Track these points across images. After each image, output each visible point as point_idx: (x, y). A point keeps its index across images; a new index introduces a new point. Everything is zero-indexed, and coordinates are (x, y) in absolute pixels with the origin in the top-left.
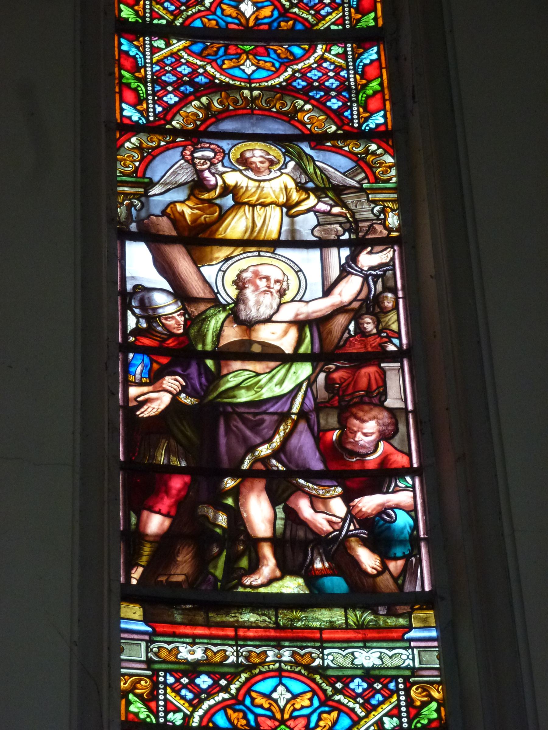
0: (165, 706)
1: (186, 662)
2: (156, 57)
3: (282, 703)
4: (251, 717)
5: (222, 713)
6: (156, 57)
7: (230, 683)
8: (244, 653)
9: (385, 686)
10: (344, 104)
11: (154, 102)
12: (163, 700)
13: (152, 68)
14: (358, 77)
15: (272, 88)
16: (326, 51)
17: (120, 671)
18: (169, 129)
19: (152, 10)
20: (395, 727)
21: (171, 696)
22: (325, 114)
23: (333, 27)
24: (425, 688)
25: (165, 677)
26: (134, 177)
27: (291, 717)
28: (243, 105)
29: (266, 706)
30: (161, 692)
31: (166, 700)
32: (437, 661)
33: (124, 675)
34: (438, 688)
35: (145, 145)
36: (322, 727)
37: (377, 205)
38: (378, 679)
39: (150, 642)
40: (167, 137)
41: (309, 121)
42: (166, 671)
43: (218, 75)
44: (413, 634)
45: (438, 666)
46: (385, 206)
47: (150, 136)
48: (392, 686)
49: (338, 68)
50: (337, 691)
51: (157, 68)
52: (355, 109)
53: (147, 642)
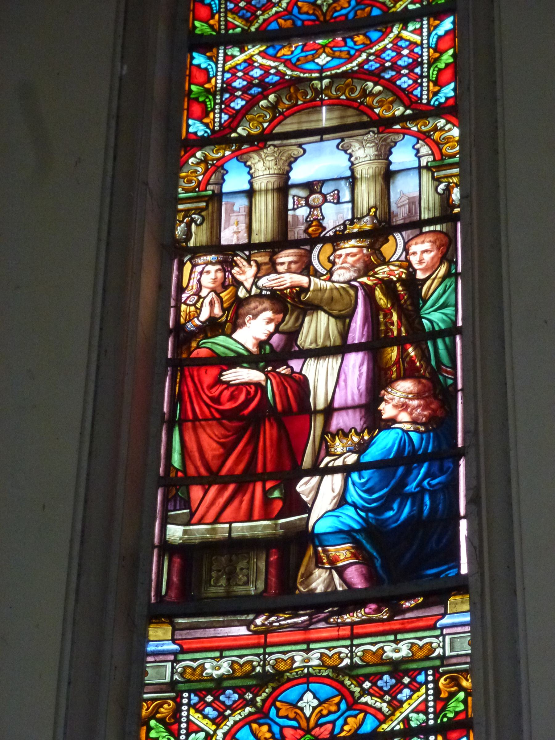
0: (187, 729)
1: (211, 679)
2: (228, 65)
3: (308, 713)
4: (276, 729)
5: (246, 729)
6: (228, 65)
7: (256, 695)
8: (271, 662)
9: (414, 679)
10: (415, 61)
11: (221, 111)
12: (186, 722)
13: (223, 76)
14: (431, 51)
15: (345, 74)
16: (402, 29)
17: (143, 697)
18: (234, 137)
19: (226, 21)
20: (421, 724)
21: (195, 717)
22: (394, 94)
23: (411, 7)
24: (454, 681)
25: (189, 698)
26: (196, 192)
27: (317, 725)
28: (313, 95)
29: (292, 715)
30: (184, 714)
31: (189, 722)
32: (470, 648)
33: (146, 700)
34: (467, 677)
35: (210, 157)
36: (346, 731)
37: (441, 182)
38: (407, 673)
39: (176, 661)
40: (233, 146)
41: (377, 104)
42: (189, 692)
43: (289, 72)
44: (446, 620)
45: (469, 652)
46: (449, 183)
47: (216, 147)
48: (421, 678)
49: (412, 45)
50: (364, 692)
51: (227, 75)
52: (425, 84)
53: (173, 662)
